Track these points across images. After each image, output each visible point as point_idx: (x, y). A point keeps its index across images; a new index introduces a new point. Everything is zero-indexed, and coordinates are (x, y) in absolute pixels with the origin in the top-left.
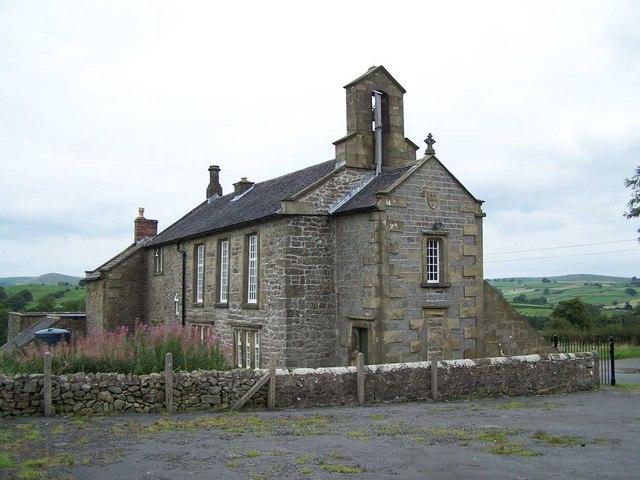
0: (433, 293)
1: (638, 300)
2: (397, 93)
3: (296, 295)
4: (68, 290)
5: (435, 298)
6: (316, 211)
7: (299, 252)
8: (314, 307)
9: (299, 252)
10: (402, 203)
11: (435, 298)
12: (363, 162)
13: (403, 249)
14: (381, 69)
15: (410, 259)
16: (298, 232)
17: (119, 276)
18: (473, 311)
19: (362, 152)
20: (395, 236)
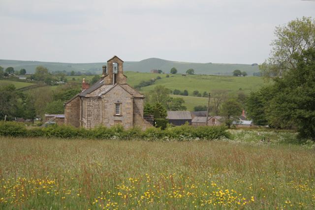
0: (117, 117)
1: (313, 113)
2: (121, 62)
3: (90, 116)
4: (159, 78)
5: (117, 118)
6: (95, 96)
7: (91, 106)
8: (95, 119)
9: (91, 106)
10: (108, 96)
11: (117, 118)
12: (109, 82)
13: (109, 107)
14: (115, 57)
15: (111, 109)
16: (90, 101)
17: (71, 105)
18: (129, 122)
19: (109, 80)
20: (106, 104)
